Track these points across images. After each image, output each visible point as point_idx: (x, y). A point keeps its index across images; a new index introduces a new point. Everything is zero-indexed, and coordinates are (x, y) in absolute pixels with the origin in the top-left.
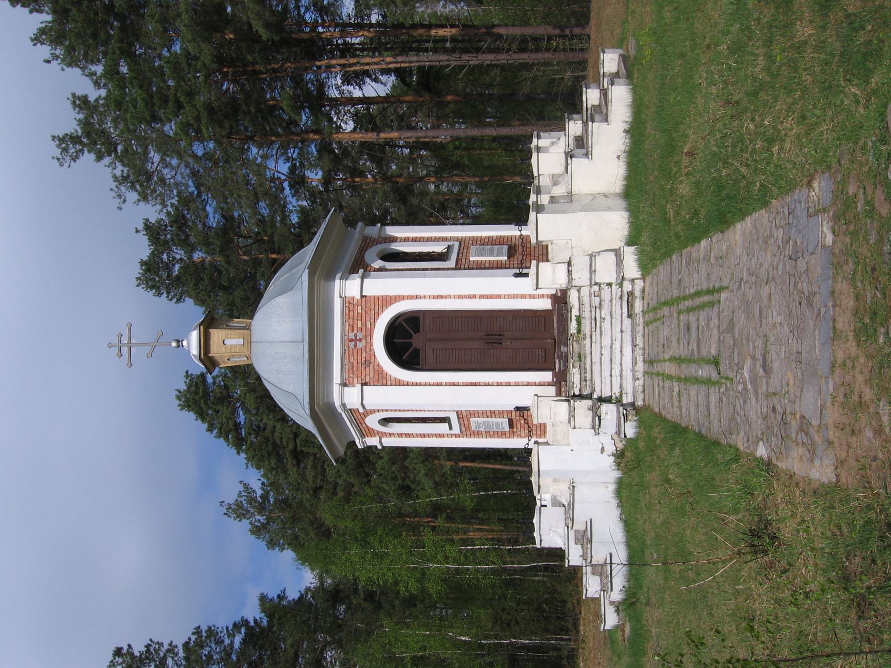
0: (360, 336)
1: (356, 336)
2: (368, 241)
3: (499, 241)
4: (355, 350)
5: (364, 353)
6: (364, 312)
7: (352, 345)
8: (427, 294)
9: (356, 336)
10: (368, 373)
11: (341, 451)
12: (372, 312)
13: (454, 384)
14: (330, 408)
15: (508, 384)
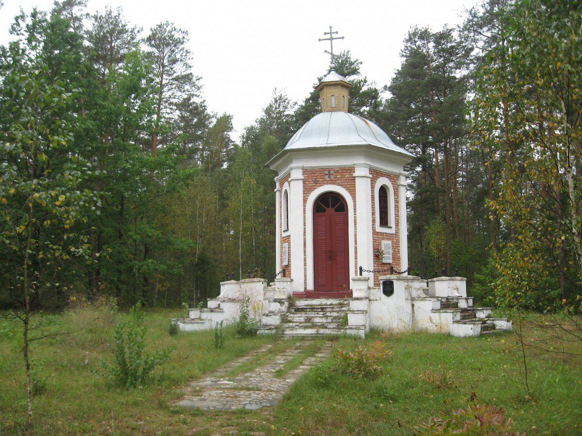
1: (332, 174)
3: (396, 257)
9: (332, 174)
11: (272, 168)
13: (305, 233)
14: (289, 161)
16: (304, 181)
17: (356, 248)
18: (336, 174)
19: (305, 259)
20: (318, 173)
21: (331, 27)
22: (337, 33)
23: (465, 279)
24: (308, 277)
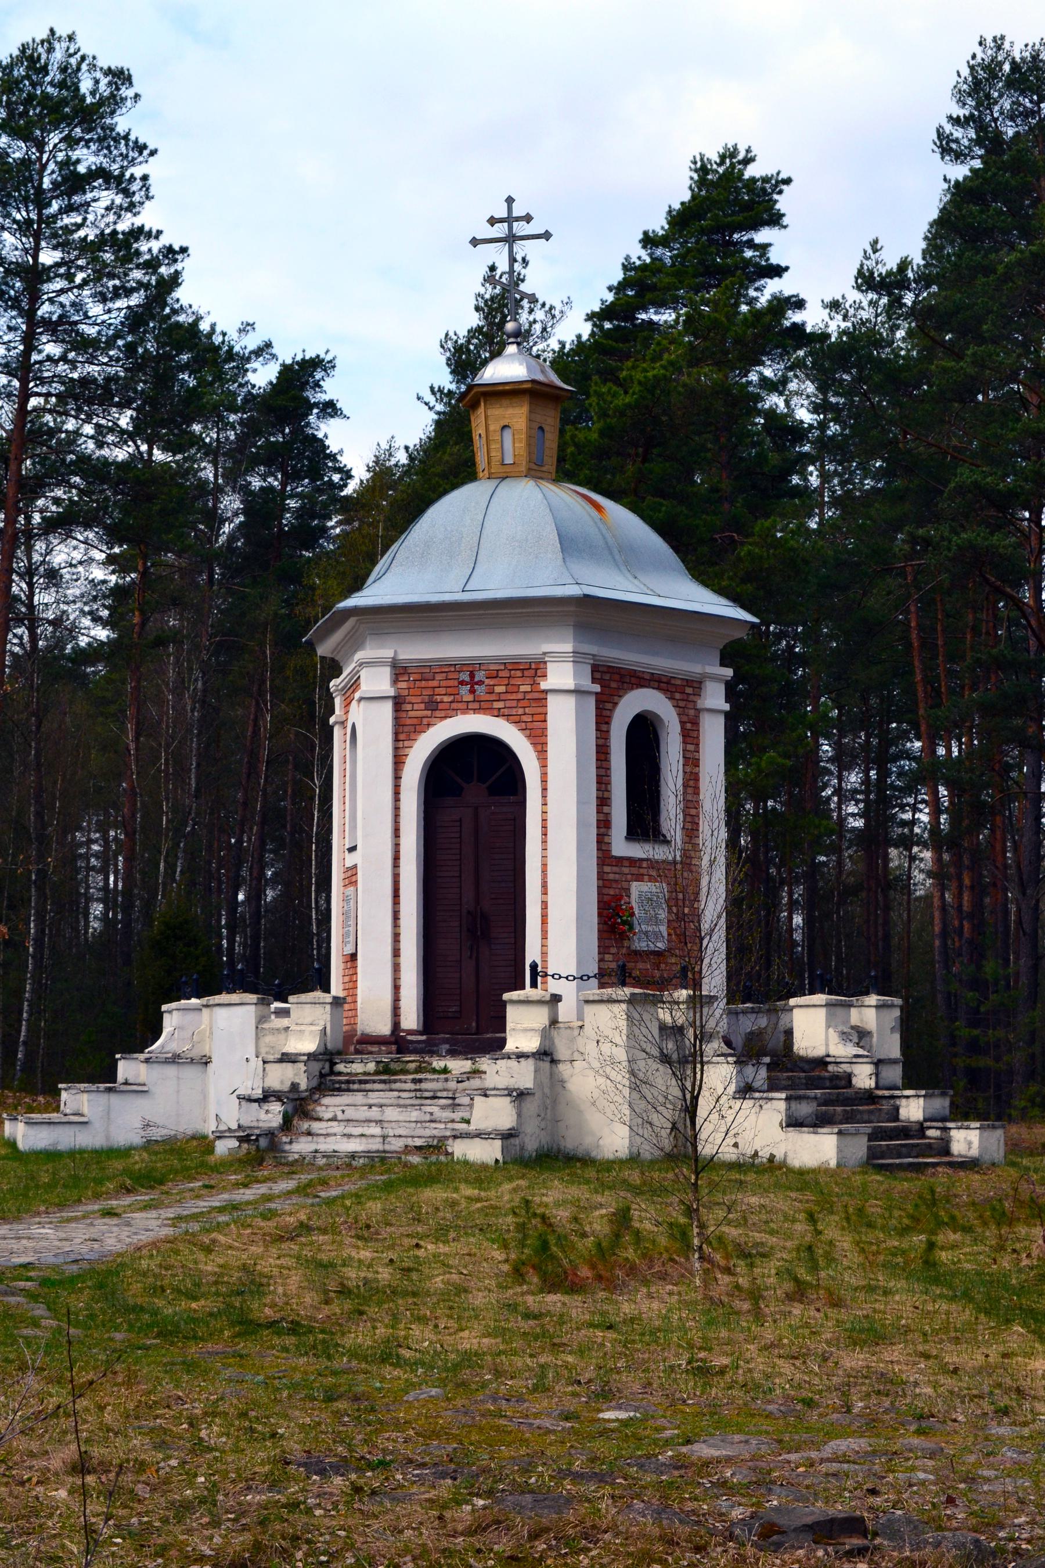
0: (480, 690)
1: (480, 683)
2: (689, 690)
4: (456, 683)
5: (451, 699)
6: (520, 696)
7: (465, 676)
8: (550, 808)
9: (480, 683)
10: (416, 707)
12: (520, 711)
14: (355, 643)
15: (396, 953)
16: (398, 703)
17: (545, 905)
18: (491, 682)
19: (396, 937)
20: (438, 677)
21: (510, 201)
22: (528, 218)
23: (898, 1001)
24: (403, 992)
